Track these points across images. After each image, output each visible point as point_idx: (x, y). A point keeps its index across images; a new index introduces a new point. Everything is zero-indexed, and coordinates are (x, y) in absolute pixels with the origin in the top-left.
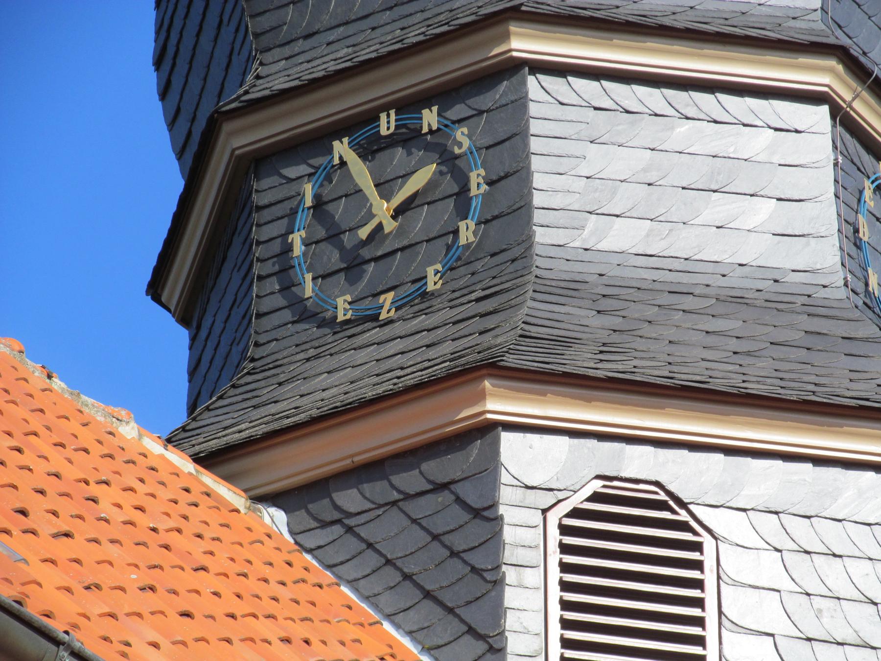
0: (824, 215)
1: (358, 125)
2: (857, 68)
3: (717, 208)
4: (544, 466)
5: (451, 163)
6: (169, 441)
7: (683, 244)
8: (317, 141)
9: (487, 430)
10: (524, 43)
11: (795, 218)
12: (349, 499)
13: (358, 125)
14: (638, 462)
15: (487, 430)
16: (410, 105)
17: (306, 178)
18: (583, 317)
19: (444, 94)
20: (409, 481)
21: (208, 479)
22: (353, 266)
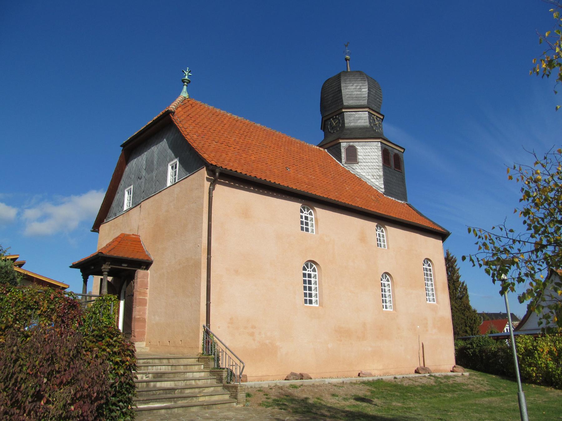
0: (368, 121)
1: (332, 117)
2: (370, 108)
3: (359, 121)
4: (344, 144)
5: (339, 120)
6: (320, 146)
7: (357, 124)
8: (330, 119)
9: (340, 143)
10: (343, 110)
11: (366, 121)
12: (331, 148)
13: (332, 117)
14: (351, 144)
15: (340, 143)
16: (336, 116)
17: (212, 364)
18: (163, 394)
19: (338, 114)
20: (335, 147)
21: (321, 149)
22: (333, 128)
